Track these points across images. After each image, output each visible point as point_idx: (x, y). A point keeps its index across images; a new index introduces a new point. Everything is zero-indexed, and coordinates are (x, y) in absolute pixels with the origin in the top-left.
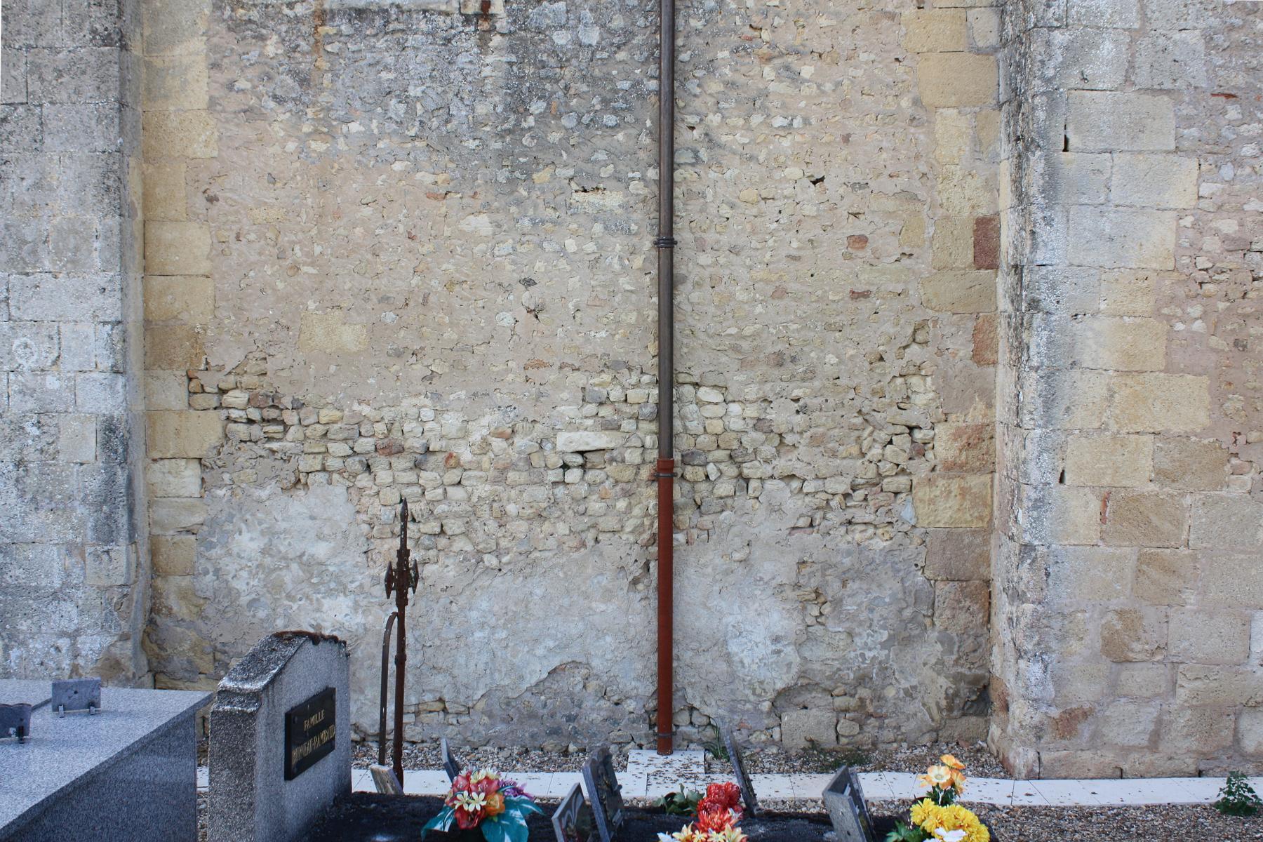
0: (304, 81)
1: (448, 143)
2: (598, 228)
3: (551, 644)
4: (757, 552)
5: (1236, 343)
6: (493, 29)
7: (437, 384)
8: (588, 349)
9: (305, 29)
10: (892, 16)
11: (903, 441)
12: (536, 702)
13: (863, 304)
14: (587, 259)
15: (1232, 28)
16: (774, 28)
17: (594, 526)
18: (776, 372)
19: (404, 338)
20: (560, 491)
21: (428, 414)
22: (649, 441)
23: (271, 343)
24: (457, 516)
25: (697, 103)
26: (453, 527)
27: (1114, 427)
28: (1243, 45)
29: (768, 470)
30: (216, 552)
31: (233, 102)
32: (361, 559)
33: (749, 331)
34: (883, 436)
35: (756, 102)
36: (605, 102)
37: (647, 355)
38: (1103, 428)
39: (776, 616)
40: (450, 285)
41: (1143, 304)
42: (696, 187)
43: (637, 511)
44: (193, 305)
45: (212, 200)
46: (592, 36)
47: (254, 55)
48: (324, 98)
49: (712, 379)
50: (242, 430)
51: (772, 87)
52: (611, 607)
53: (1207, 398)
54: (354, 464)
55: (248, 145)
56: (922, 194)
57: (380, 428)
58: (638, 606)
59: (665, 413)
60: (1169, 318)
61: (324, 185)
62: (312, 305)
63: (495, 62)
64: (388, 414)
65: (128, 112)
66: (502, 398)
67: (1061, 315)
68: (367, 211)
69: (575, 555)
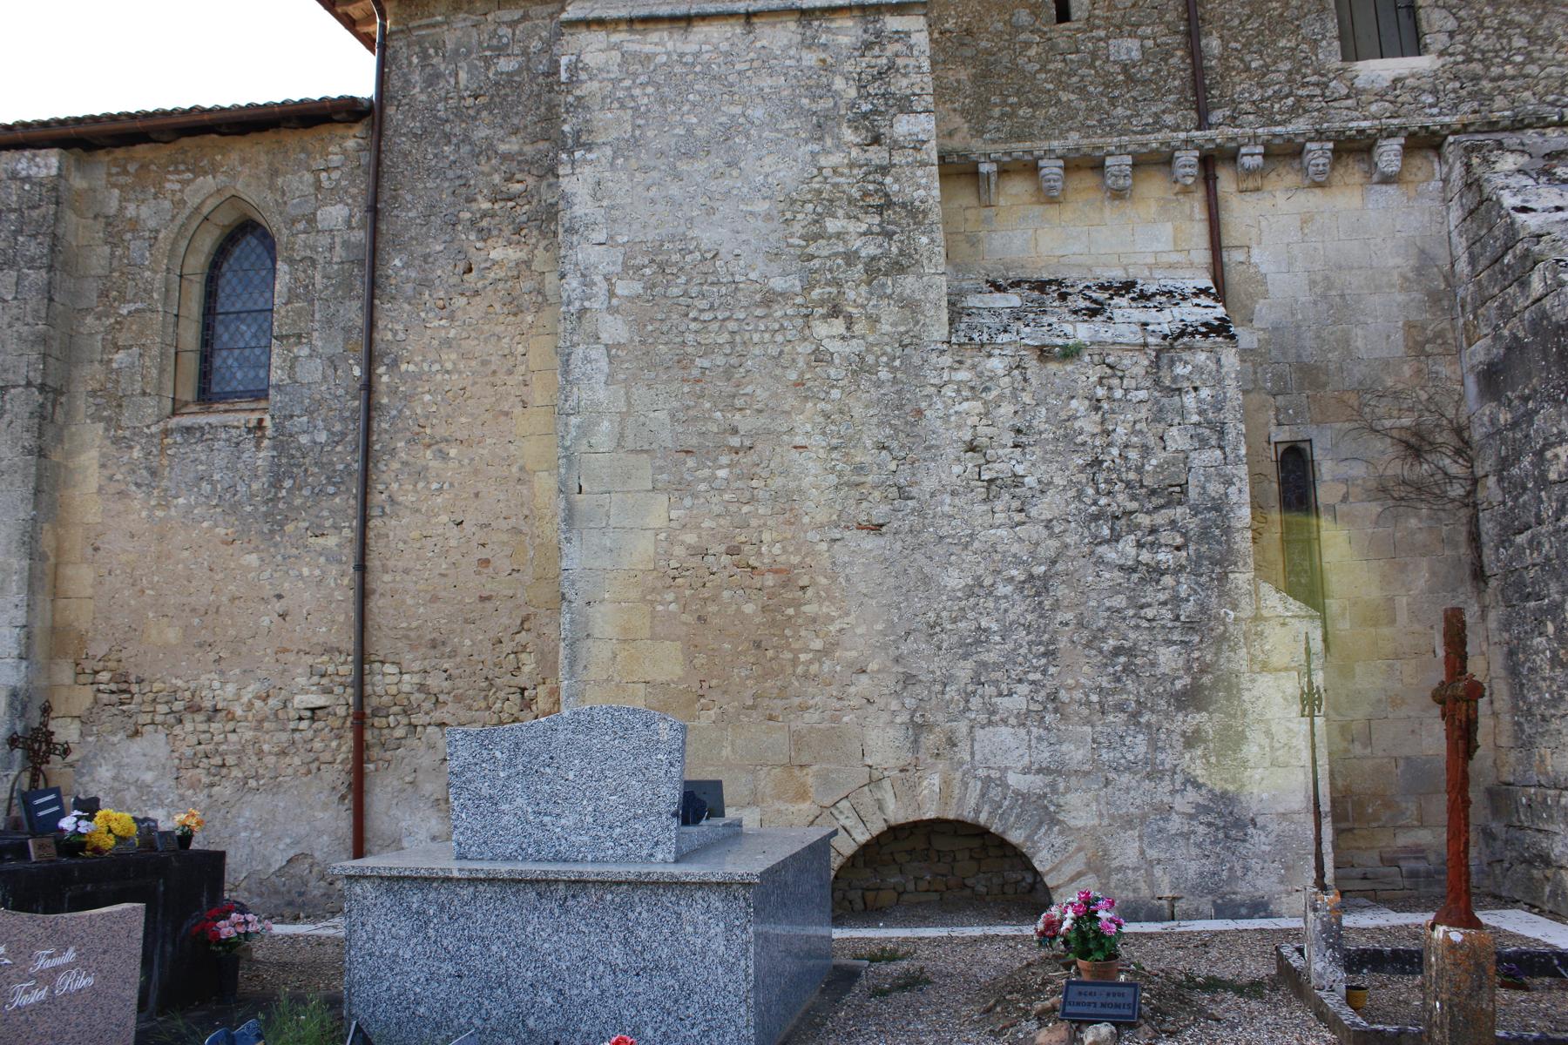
0: (153, 473)
1: (235, 508)
2: (322, 560)
3: (288, 841)
4: (421, 777)
5: (699, 618)
6: (263, 436)
7: (223, 665)
8: (314, 640)
9: (156, 441)
10: (506, 414)
11: (516, 698)
12: (279, 881)
13: (489, 605)
14: (313, 580)
15: (688, 408)
16: (433, 426)
17: (317, 759)
18: (432, 652)
19: (205, 635)
20: (297, 736)
21: (216, 684)
22: (351, 701)
23: (126, 640)
24: (233, 753)
25: (384, 477)
26: (231, 760)
27: (617, 679)
28: (696, 419)
29: (427, 719)
30: (86, 779)
31: (112, 488)
32: (173, 783)
33: (414, 624)
34: (502, 694)
35: (421, 474)
36: (328, 478)
37: (349, 644)
38: (609, 680)
39: (434, 822)
40: (233, 599)
41: (634, 594)
42: (383, 531)
43: (344, 749)
44: (80, 614)
45: (96, 549)
46: (322, 437)
47: (125, 459)
48: (164, 483)
49: (391, 658)
50: (105, 698)
51: (431, 464)
52: (327, 815)
53: (681, 657)
54: (171, 719)
55: (119, 514)
56: (525, 529)
57: (188, 694)
58: (344, 814)
59: (360, 683)
60: (652, 602)
61: (162, 538)
62: (151, 615)
63: (264, 456)
64: (193, 685)
65: (44, 497)
66: (261, 673)
67: (578, 603)
68: (186, 554)
69: (305, 779)
